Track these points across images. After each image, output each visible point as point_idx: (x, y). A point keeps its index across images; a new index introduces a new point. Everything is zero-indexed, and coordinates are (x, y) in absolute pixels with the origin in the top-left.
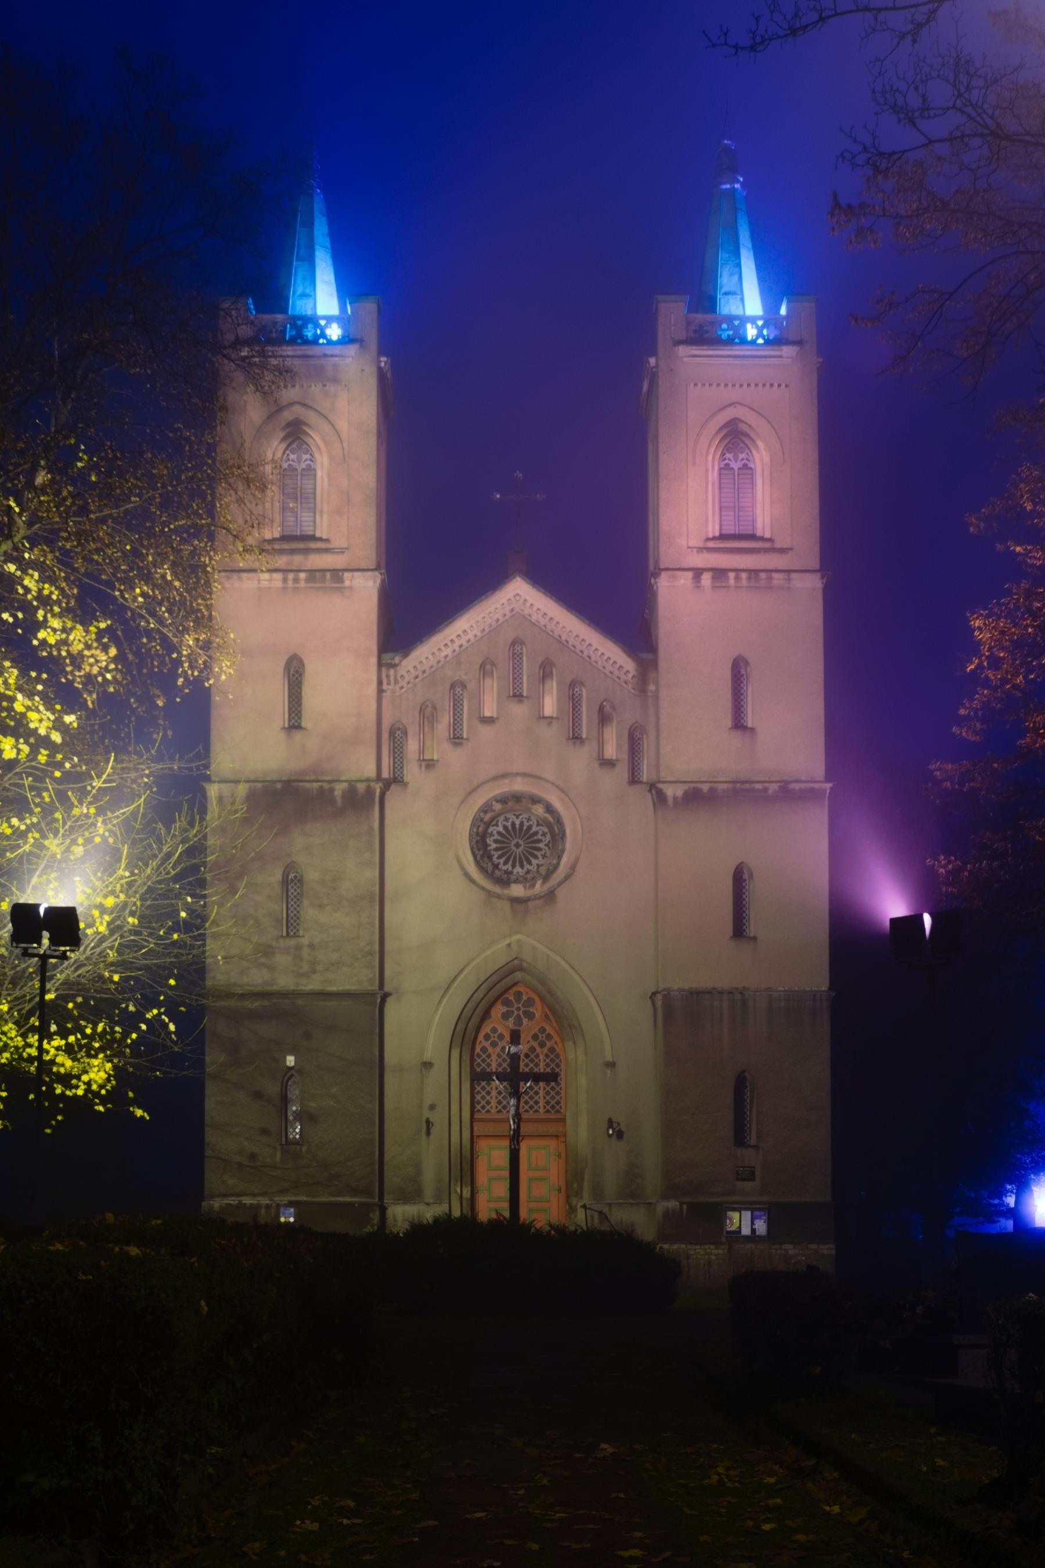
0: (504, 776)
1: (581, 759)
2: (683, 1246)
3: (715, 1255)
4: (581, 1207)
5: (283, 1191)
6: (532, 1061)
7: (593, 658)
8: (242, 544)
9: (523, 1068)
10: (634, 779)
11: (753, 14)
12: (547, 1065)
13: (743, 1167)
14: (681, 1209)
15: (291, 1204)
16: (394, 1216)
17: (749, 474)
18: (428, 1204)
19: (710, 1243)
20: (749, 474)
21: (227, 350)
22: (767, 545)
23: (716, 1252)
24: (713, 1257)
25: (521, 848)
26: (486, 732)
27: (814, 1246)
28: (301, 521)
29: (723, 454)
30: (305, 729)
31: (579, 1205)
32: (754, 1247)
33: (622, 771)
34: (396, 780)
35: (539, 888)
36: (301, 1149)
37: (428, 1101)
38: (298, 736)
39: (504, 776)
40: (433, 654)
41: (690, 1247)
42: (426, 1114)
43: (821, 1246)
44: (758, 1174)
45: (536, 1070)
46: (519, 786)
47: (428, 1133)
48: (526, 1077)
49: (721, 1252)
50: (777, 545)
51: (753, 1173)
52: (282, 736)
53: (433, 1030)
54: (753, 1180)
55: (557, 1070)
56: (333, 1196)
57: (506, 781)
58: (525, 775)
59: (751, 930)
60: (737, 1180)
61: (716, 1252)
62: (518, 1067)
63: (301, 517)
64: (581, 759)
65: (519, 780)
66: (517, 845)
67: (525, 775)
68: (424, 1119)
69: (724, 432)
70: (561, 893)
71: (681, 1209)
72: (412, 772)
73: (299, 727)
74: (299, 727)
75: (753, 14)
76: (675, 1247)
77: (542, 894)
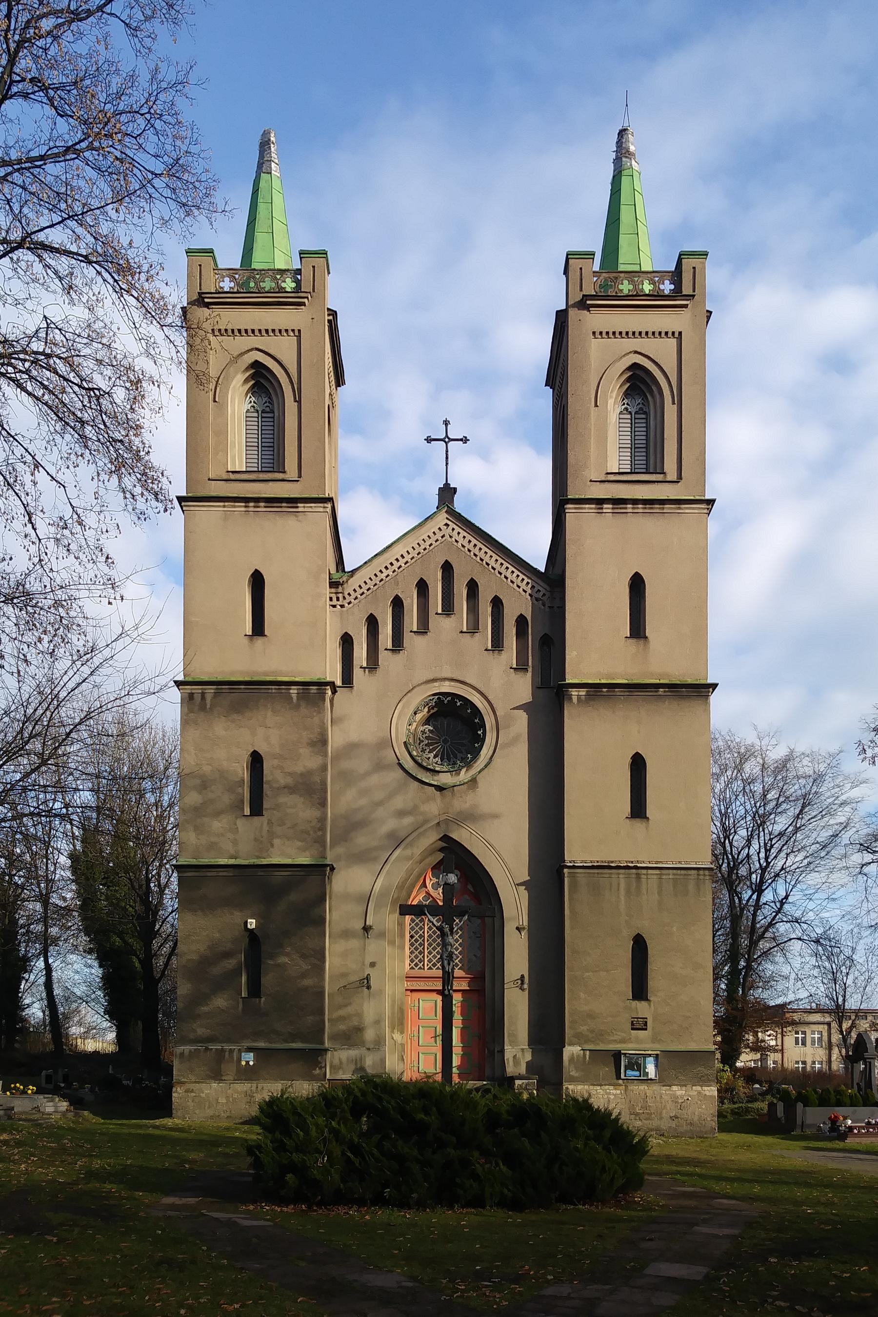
0: (434, 680)
8: (187, 1053)
13: (637, 1018)
14: (584, 1055)
15: (249, 1050)
17: (655, 468)
18: (369, 1049)
20: (655, 468)
21: (51, 25)
23: (614, 1092)
24: (612, 1097)
27: (699, 1088)
28: (258, 418)
36: (260, 1001)
37: (369, 960)
38: (259, 641)
39: (434, 680)
40: (376, 575)
41: (591, 1087)
43: (705, 1088)
49: (619, 1092)
51: (646, 1024)
52: (246, 641)
54: (646, 1029)
55: (333, 590)
56: (286, 1041)
57: (436, 684)
58: (452, 680)
60: (633, 1029)
61: (614, 1092)
63: (258, 422)
65: (447, 683)
67: (452, 680)
70: (481, 781)
71: (584, 1055)
76: (580, 1087)
77: (466, 781)
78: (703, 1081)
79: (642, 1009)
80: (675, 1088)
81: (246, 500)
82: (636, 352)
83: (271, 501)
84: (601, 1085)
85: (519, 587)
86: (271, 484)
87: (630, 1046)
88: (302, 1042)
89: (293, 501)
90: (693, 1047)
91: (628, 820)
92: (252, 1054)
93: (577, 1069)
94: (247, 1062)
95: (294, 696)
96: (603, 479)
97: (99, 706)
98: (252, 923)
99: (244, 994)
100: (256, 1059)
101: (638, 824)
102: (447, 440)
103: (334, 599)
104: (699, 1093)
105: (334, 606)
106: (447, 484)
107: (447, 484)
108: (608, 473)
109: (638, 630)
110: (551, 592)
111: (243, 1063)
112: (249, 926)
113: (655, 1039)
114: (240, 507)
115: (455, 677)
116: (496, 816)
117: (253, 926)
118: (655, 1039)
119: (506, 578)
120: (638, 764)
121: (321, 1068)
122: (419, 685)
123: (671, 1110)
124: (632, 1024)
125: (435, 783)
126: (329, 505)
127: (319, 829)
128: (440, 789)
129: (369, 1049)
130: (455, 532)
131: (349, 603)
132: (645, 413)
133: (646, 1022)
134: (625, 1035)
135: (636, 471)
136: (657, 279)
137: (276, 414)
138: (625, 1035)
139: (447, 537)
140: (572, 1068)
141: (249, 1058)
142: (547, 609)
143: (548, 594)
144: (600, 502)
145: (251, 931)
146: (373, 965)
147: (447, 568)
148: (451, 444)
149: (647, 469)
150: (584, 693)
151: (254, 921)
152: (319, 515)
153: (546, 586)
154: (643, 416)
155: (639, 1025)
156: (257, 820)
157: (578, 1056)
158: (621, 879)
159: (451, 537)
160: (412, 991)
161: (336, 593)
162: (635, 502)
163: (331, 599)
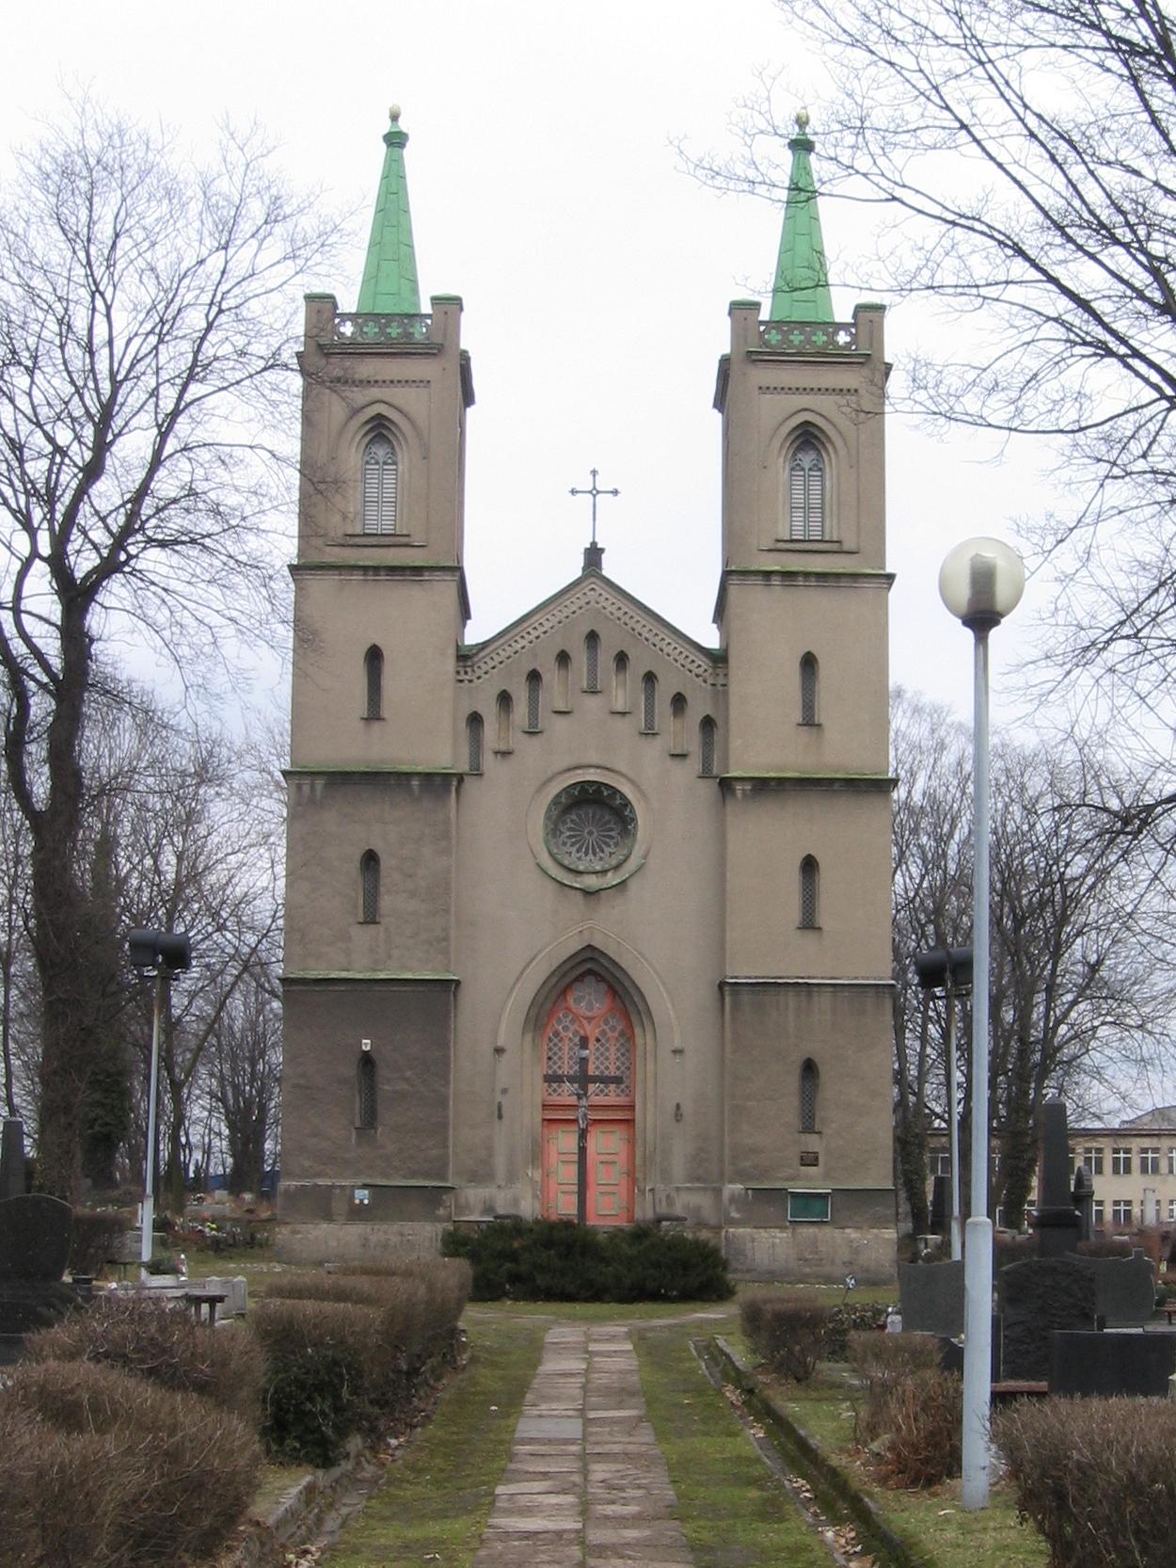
1: (653, 752)
2: (749, 1230)
3: (780, 1238)
4: (650, 1190)
5: (358, 1173)
6: (603, 1045)
7: (666, 650)
9: (591, 1071)
10: (706, 774)
11: (395, 117)
12: (618, 1068)
15: (365, 1186)
16: (467, 1199)
17: (945, 1135)
19: (776, 1227)
22: (835, 547)
24: (778, 1241)
25: (595, 834)
26: (561, 722)
27: (875, 1231)
29: (794, 454)
30: (383, 719)
31: (647, 1188)
32: (817, 1230)
33: (694, 764)
34: (477, 772)
35: (612, 879)
37: (499, 1086)
38: (376, 726)
42: (499, 1097)
44: (821, 1159)
45: (607, 1073)
46: (592, 775)
47: (500, 1117)
48: (594, 1080)
50: (846, 547)
51: (817, 1159)
53: (506, 1015)
55: (461, 664)
57: (579, 772)
59: (824, 919)
61: (780, 1235)
62: (587, 1071)
64: (653, 752)
65: (592, 770)
66: (590, 833)
68: (496, 1103)
69: (792, 437)
70: (633, 886)
71: (747, 1193)
72: (488, 761)
73: (379, 719)
74: (379, 719)
75: (395, 117)
76: (742, 1230)
77: (603, 987)
78: (879, 1222)
79: (813, 1143)
80: (848, 1231)
81: (365, 569)
82: (806, 410)
83: (392, 570)
84: (765, 1228)
85: (676, 661)
86: (393, 549)
87: (799, 1183)
88: (424, 1179)
89: (418, 570)
90: (869, 1185)
91: (798, 931)
92: (366, 1192)
93: (738, 1210)
94: (362, 1201)
95: (416, 789)
96: (772, 547)
97: (66, 282)
98: (366, 1044)
99: (358, 1124)
100: (371, 1198)
101: (811, 935)
102: (595, 492)
103: (462, 673)
104: (877, 1236)
105: (461, 681)
106: (594, 544)
107: (594, 544)
108: (778, 541)
109: (809, 721)
110: (715, 668)
111: (357, 1202)
112: (364, 1048)
113: (827, 1175)
114: (358, 577)
115: (601, 763)
116: (593, 555)
117: (368, 1048)
118: (827, 1175)
119: (662, 650)
120: (809, 865)
121: (445, 1208)
122: (560, 773)
123: (845, 1254)
124: (802, 1158)
125: (578, 886)
126: (458, 574)
127: (444, 939)
128: (587, 893)
129: (499, 1187)
130: (602, 599)
131: (479, 678)
132: (820, 470)
133: (817, 1158)
134: (791, 1171)
135: (811, 538)
136: (831, 330)
137: (400, 468)
138: (791, 1171)
139: (593, 603)
140: (733, 1208)
141: (362, 1196)
142: (710, 687)
143: (710, 670)
144: (767, 575)
145: (366, 1053)
146: (504, 1091)
147: (592, 637)
148: (590, 489)
149: (822, 535)
150: (749, 787)
151: (369, 1041)
152: (447, 589)
153: (707, 661)
154: (819, 473)
155: (810, 1160)
156: (372, 929)
157: (740, 1195)
158: (791, 1000)
159: (598, 603)
160: (549, 1120)
161: (465, 667)
162: (807, 575)
163: (458, 673)
